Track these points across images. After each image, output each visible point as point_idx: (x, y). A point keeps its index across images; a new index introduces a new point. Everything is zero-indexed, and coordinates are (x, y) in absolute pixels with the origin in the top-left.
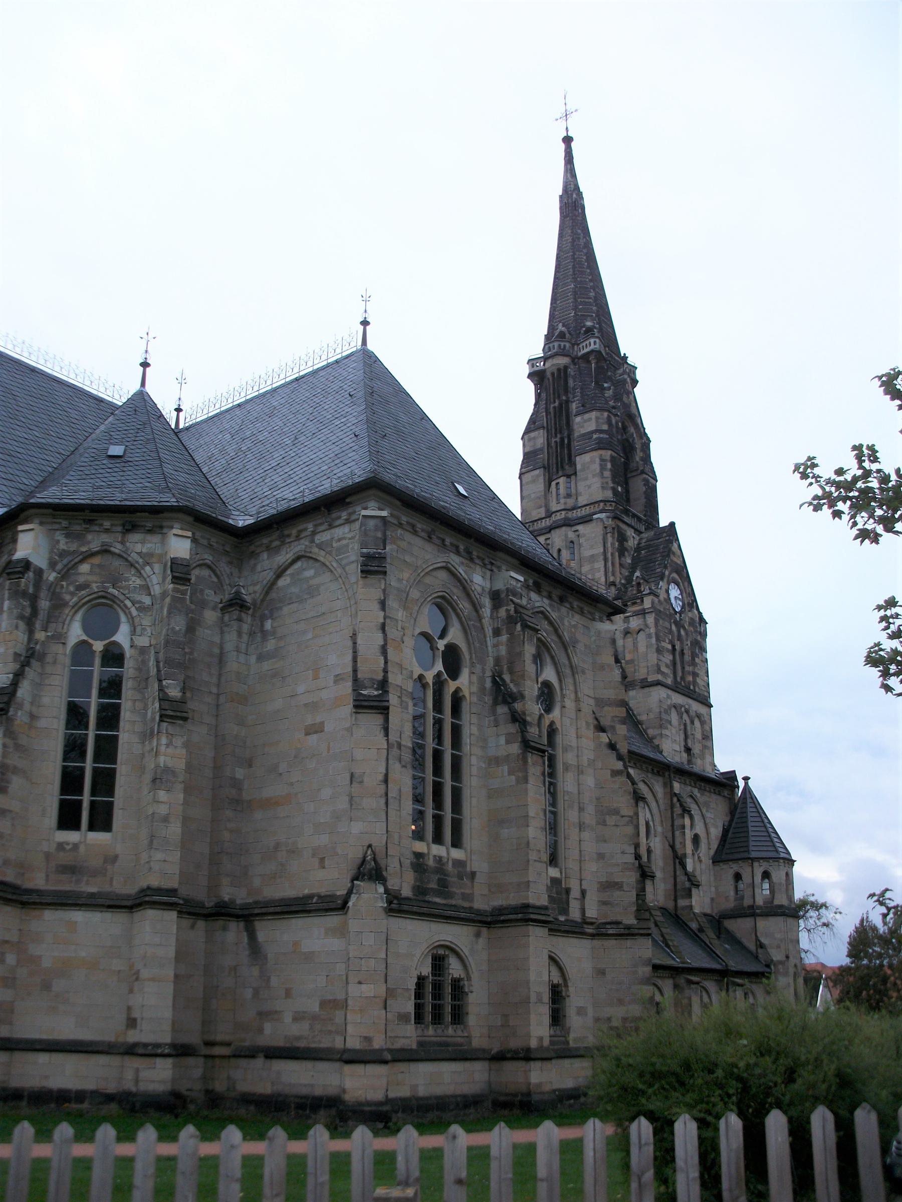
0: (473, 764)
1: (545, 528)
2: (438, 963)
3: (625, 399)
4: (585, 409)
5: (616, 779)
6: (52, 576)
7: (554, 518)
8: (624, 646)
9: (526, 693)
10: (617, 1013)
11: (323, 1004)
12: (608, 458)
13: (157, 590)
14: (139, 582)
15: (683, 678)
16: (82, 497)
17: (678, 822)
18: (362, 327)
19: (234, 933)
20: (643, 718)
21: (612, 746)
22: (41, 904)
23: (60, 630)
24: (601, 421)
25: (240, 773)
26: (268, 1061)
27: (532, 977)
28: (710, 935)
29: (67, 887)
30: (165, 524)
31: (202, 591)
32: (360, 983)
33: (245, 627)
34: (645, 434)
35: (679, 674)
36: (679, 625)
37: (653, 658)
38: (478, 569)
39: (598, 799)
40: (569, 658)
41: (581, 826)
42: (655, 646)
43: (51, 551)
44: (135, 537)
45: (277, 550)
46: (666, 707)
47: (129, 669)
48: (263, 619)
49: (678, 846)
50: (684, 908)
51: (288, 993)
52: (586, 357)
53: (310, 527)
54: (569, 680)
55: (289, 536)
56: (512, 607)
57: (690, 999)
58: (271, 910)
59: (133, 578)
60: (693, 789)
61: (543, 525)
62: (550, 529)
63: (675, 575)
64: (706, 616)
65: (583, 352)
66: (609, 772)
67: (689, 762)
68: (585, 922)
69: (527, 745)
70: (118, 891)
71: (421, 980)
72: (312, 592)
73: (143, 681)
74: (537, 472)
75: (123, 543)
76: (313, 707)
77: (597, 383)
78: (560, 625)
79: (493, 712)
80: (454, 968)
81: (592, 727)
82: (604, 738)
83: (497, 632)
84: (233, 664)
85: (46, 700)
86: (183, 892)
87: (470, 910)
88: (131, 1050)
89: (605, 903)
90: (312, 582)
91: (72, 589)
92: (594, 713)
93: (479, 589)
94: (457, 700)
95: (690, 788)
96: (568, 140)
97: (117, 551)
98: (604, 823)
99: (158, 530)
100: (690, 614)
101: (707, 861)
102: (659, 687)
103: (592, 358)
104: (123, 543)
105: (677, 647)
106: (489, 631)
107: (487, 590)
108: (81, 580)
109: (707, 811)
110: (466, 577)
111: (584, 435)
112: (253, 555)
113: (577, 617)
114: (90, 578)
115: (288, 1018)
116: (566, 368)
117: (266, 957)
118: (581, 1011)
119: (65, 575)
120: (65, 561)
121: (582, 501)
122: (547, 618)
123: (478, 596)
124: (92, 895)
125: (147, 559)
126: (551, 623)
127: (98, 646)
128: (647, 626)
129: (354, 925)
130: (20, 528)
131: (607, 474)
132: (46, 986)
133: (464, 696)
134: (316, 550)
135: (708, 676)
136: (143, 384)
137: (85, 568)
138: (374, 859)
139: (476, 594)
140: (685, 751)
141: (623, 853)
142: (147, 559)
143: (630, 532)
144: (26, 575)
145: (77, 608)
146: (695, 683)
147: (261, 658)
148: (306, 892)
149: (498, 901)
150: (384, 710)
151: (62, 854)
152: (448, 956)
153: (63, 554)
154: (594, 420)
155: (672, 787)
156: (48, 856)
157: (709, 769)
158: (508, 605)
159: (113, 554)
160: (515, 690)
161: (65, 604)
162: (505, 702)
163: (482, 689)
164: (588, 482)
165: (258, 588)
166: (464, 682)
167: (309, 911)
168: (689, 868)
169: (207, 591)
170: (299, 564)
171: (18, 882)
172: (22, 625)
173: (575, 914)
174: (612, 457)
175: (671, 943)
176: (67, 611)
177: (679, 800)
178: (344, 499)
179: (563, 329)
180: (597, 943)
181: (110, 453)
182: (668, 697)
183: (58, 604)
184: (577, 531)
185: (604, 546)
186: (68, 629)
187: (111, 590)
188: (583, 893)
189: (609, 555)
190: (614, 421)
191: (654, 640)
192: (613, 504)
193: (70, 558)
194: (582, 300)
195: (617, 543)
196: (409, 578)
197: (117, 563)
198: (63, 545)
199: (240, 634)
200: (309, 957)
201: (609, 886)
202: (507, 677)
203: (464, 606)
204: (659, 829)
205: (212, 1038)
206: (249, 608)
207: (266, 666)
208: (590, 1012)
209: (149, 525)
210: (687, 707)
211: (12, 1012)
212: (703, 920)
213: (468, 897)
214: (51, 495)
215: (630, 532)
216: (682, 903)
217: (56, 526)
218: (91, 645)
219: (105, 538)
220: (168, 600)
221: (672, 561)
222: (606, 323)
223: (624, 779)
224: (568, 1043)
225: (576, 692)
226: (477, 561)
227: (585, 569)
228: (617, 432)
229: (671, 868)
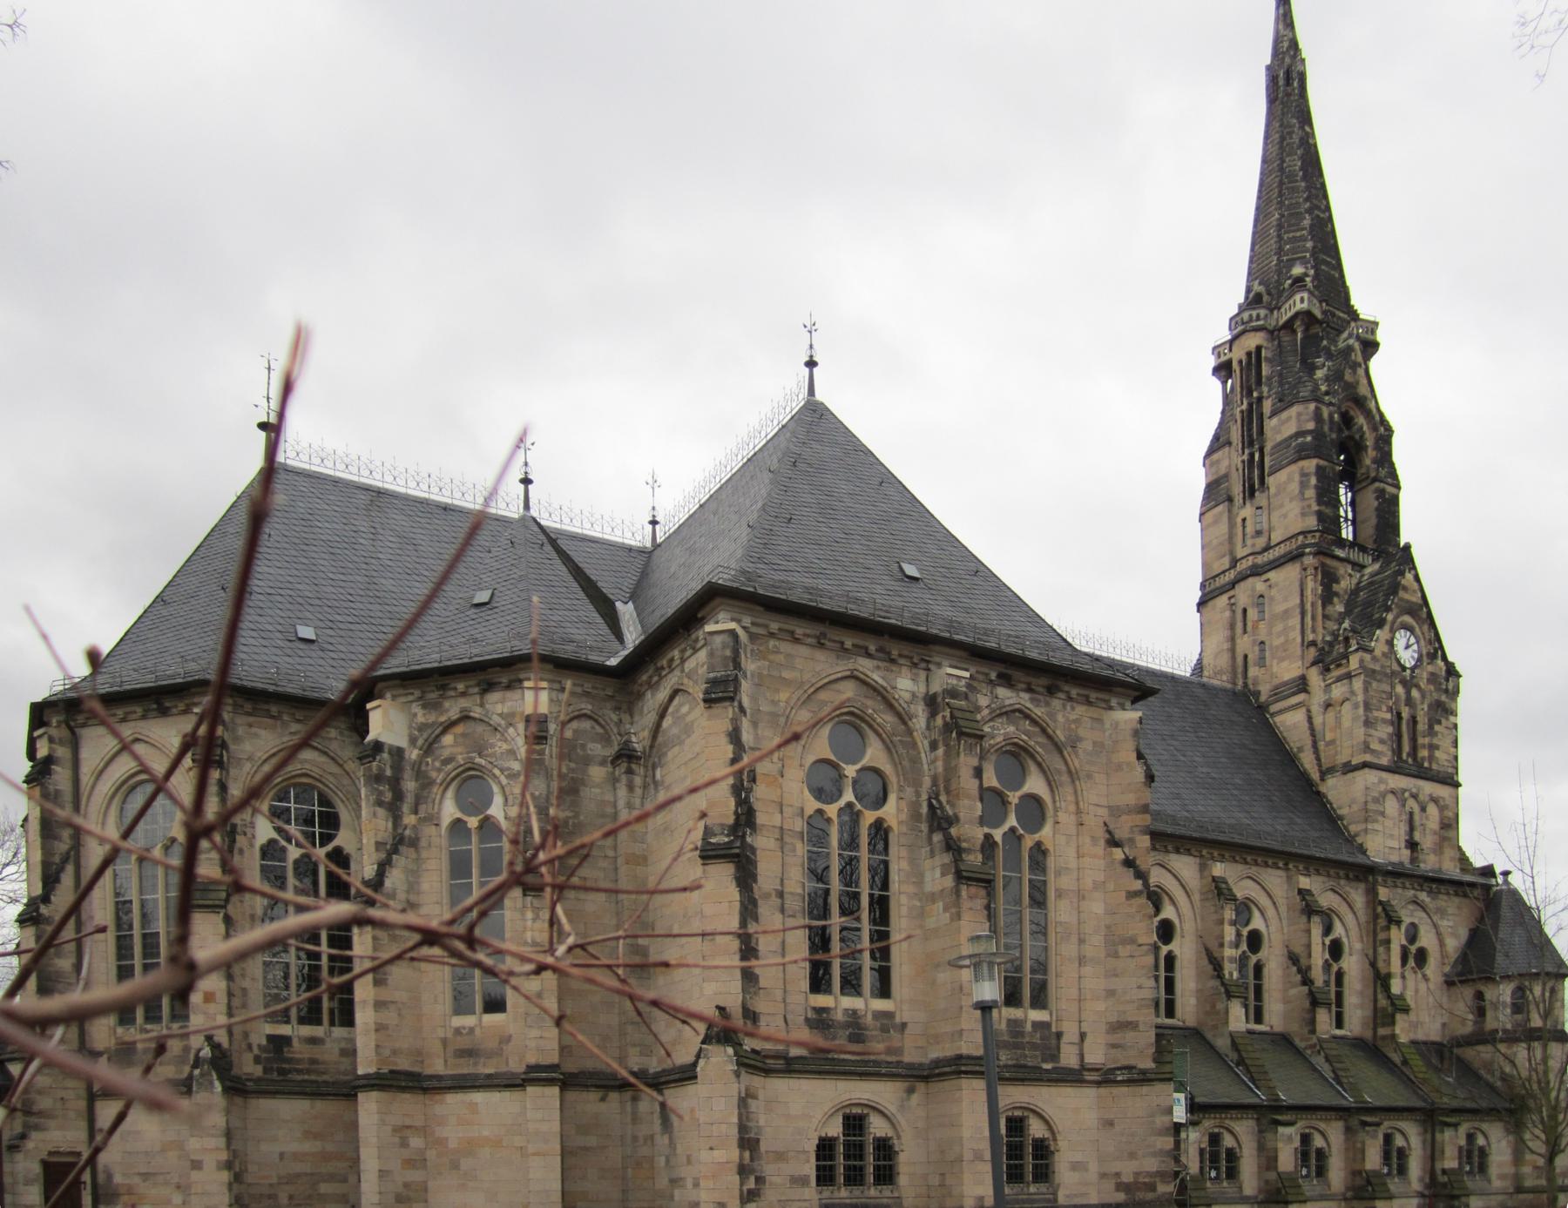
1: (1228, 584)
4: (1283, 403)
5: (1133, 901)
6: (414, 754)
7: (1239, 567)
8: (1324, 724)
9: (961, 815)
10: (1128, 1169)
12: (1313, 470)
14: (505, 746)
16: (432, 660)
17: (1382, 936)
18: (807, 370)
20: (1343, 812)
21: (1129, 863)
22: (440, 1088)
23: (430, 811)
24: (1303, 417)
27: (966, 1133)
29: (465, 1071)
30: (522, 676)
31: (583, 746)
32: (711, 1149)
37: (1360, 732)
38: (905, 670)
39: (1108, 927)
40: (1066, 763)
41: (1081, 961)
42: (1363, 718)
43: (410, 727)
44: (493, 697)
46: (1377, 795)
49: (1381, 965)
50: (1384, 1038)
51: (689, 1162)
52: (1289, 326)
53: (676, 653)
56: (947, 713)
57: (1363, 1143)
58: (672, 1077)
59: (499, 744)
60: (1419, 893)
61: (1227, 579)
62: (1233, 584)
63: (1407, 619)
65: (1285, 318)
66: (1124, 894)
67: (1413, 860)
68: (1084, 1068)
69: (961, 877)
70: (514, 1070)
74: (1221, 508)
75: (482, 705)
77: (1304, 361)
78: (1049, 722)
80: (877, 1127)
81: (1102, 842)
82: (1118, 854)
83: (934, 746)
85: (425, 886)
89: (1114, 1046)
91: (437, 764)
92: (1105, 824)
93: (907, 696)
95: (1412, 892)
97: (477, 716)
98: (1116, 955)
99: (514, 685)
100: (1430, 668)
102: (1367, 770)
104: (482, 705)
107: (921, 696)
108: (446, 753)
109: (1442, 918)
110: (885, 684)
111: (1280, 444)
112: (640, 696)
113: (1081, 710)
114: (455, 750)
116: (1259, 348)
118: (1076, 1166)
119: (429, 749)
120: (425, 735)
122: (1027, 717)
123: (905, 706)
124: (489, 1076)
125: (509, 718)
126: (1034, 722)
127: (473, 822)
128: (1353, 693)
130: (369, 706)
131: (1311, 493)
132: (455, 1166)
133: (889, 827)
135: (1456, 747)
136: (527, 506)
137: (448, 739)
139: (901, 702)
140: (1406, 847)
141: (1140, 987)
143: (1343, 570)
144: (378, 758)
149: (935, 1053)
151: (459, 1038)
152: (868, 1114)
153: (422, 728)
154: (1294, 421)
155: (1376, 894)
156: (444, 1042)
158: (944, 710)
159: (474, 719)
160: (951, 813)
161: (431, 783)
162: (940, 828)
164: (1284, 511)
165: (646, 733)
166: (892, 812)
169: (590, 745)
170: (676, 701)
171: (416, 1069)
174: (1319, 468)
175: (1345, 1080)
176: (435, 790)
177: (1384, 909)
178: (695, 616)
180: (1103, 1091)
182: (1381, 781)
183: (425, 783)
184: (1268, 580)
185: (1302, 595)
186: (440, 809)
187: (478, 760)
189: (1308, 607)
190: (1325, 415)
191: (1361, 711)
192: (1318, 534)
193: (429, 731)
194: (1291, 235)
195: (1320, 588)
196: (790, 698)
197: (480, 728)
198: (420, 719)
199: (631, 788)
202: (943, 798)
204: (1358, 946)
206: (640, 758)
208: (1094, 1168)
210: (1414, 790)
211: (426, 1190)
214: (395, 664)
216: (1382, 1031)
217: (411, 698)
218: (465, 823)
219: (463, 703)
221: (1401, 600)
222: (1328, 264)
224: (1056, 1200)
225: (1077, 803)
226: (902, 661)
228: (1331, 429)
229: (1371, 991)
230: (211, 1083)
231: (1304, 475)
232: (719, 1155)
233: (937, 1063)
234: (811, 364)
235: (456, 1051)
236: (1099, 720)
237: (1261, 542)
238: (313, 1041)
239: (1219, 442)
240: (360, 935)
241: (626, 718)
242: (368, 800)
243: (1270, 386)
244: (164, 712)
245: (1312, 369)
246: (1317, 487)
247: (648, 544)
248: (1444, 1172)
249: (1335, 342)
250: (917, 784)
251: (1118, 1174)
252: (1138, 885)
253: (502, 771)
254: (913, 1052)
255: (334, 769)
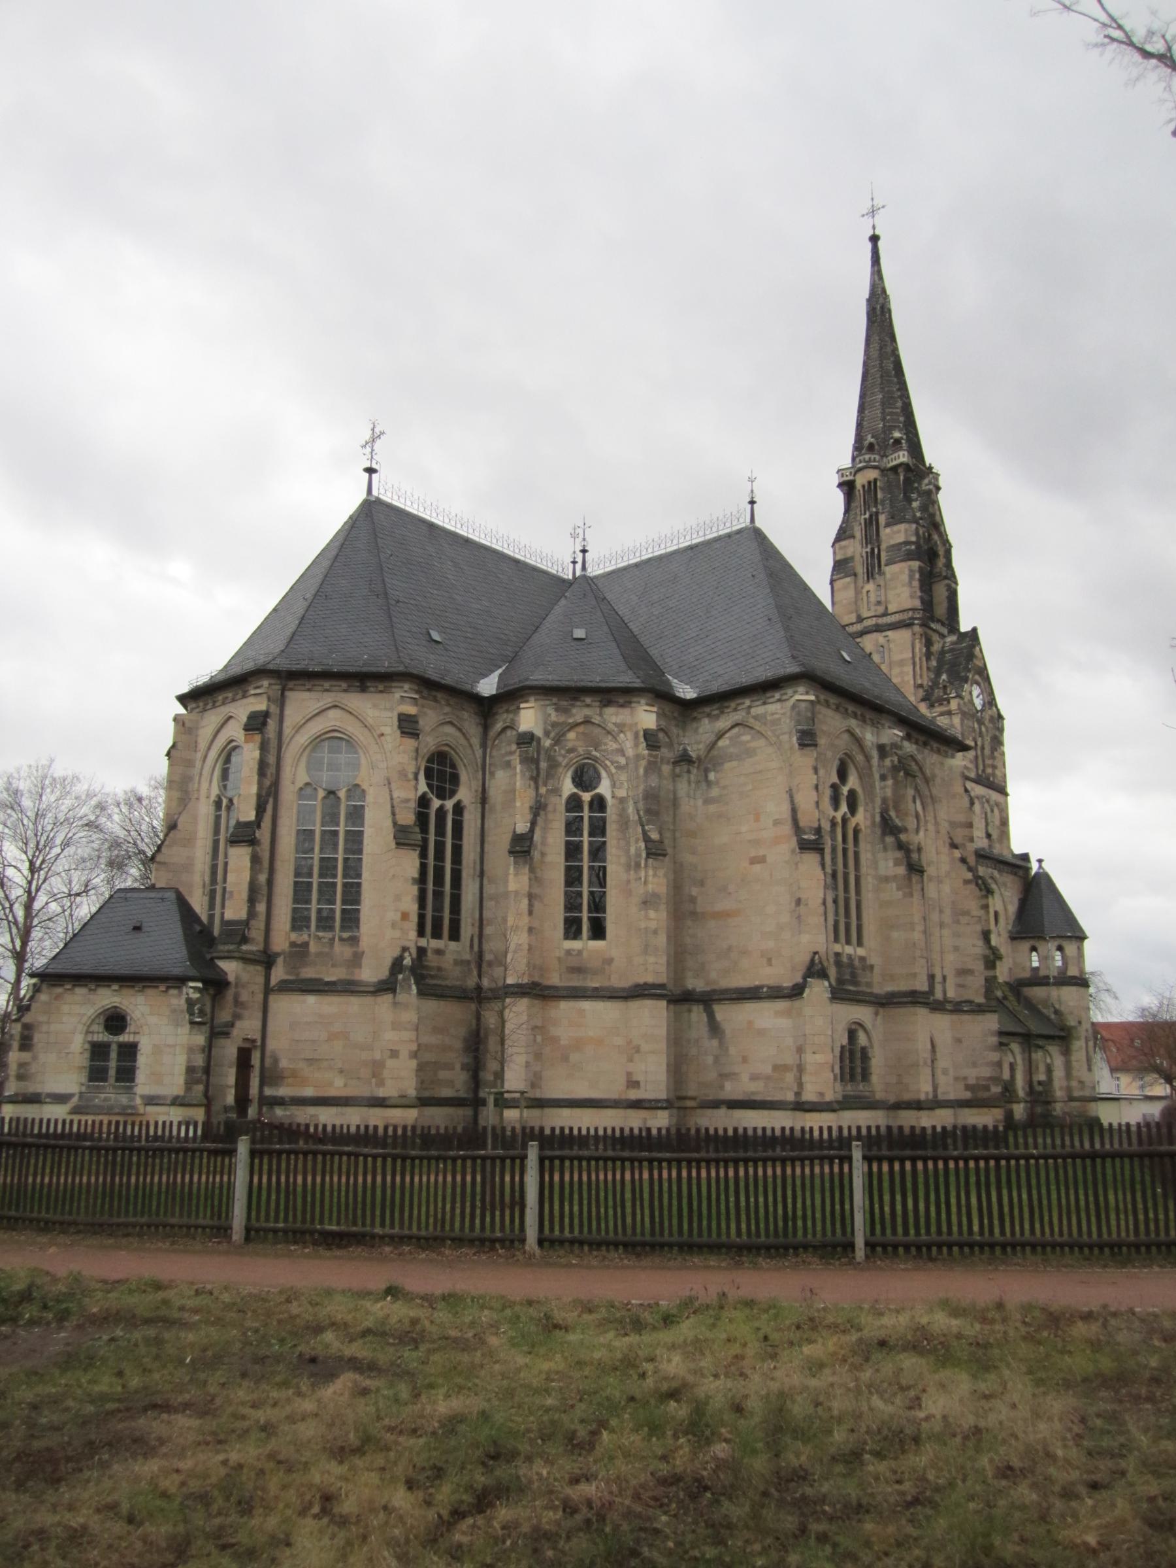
0: (868, 883)
2: (852, 1035)
3: (931, 510)
4: (894, 520)
11: (776, 1068)
13: (630, 752)
14: (615, 746)
15: (984, 771)
19: (697, 1014)
21: (963, 860)
25: (694, 891)
26: (730, 1111)
28: (1012, 1003)
33: (692, 777)
34: (948, 541)
35: (981, 767)
36: (980, 722)
39: (953, 902)
41: (942, 925)
43: (545, 723)
45: (717, 717)
47: (611, 813)
48: (707, 771)
51: (745, 1060)
52: (894, 469)
53: (747, 702)
54: (930, 808)
55: (727, 707)
56: (896, 759)
62: (862, 634)
63: (977, 677)
64: (1003, 713)
67: (990, 846)
68: (946, 1000)
71: (842, 1047)
72: (750, 753)
73: (624, 823)
75: (601, 715)
76: (757, 842)
79: (883, 841)
80: (862, 1039)
82: (957, 854)
83: (883, 778)
84: (685, 807)
85: (550, 840)
86: (670, 986)
87: (871, 994)
88: (637, 1105)
90: (748, 745)
91: (563, 752)
94: (856, 832)
96: (874, 239)
98: (958, 922)
100: (990, 712)
101: (1005, 935)
103: (900, 470)
104: (601, 715)
105: (979, 743)
106: (877, 776)
108: (570, 745)
111: (893, 546)
115: (745, 1078)
116: (875, 480)
117: (723, 1032)
119: (558, 741)
120: (557, 730)
121: (891, 609)
124: (596, 989)
125: (621, 727)
127: (586, 797)
129: (808, 1011)
130: (522, 705)
131: (916, 584)
132: (565, 1059)
134: (751, 720)
137: (571, 735)
138: (821, 962)
141: (974, 946)
142: (621, 727)
143: (935, 637)
145: (567, 766)
146: (994, 775)
147: (707, 801)
148: (757, 983)
149: (890, 988)
150: (821, 851)
153: (554, 725)
156: (559, 959)
157: (1005, 853)
159: (593, 723)
163: (873, 823)
166: (861, 818)
167: (760, 998)
168: (993, 943)
170: (736, 730)
172: (532, 783)
173: (939, 995)
174: (920, 567)
179: (872, 440)
180: (955, 1017)
181: (575, 636)
183: (554, 765)
187: (594, 753)
188: (944, 978)
189: (917, 660)
190: (921, 532)
197: (597, 730)
199: (689, 782)
200: (761, 1032)
201: (963, 972)
202: (893, 814)
203: (860, 758)
205: (684, 1094)
207: (712, 808)
208: (951, 1072)
209: (621, 701)
212: (1006, 989)
213: (869, 985)
215: (935, 637)
217: (548, 702)
219: (587, 712)
220: (643, 763)
223: (973, 886)
227: (896, 671)
230: (410, 986)
231: (911, 571)
232: (820, 1058)
233: (893, 995)
234: (752, 502)
235: (568, 968)
236: (942, 764)
237: (881, 610)
238: (439, 952)
239: (843, 534)
240: (516, 874)
241: (681, 733)
242: (523, 775)
243: (883, 505)
244: (363, 689)
245: (909, 500)
246: (920, 580)
247: (571, 577)
248: (1040, 1083)
249: (920, 484)
250: (873, 801)
251: (965, 1078)
252: (969, 876)
253: (612, 763)
254: (882, 987)
255: (463, 741)
